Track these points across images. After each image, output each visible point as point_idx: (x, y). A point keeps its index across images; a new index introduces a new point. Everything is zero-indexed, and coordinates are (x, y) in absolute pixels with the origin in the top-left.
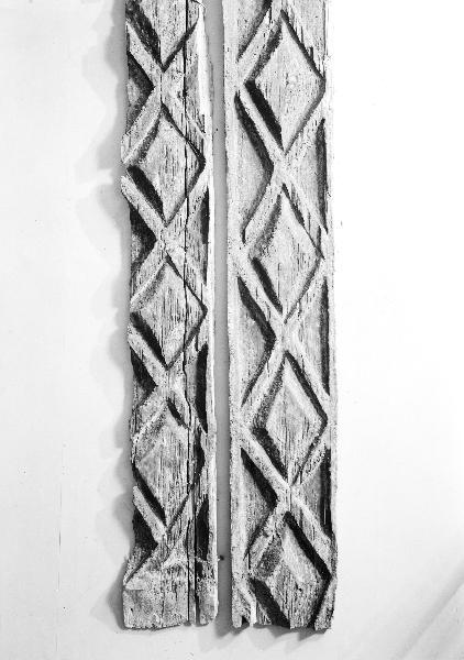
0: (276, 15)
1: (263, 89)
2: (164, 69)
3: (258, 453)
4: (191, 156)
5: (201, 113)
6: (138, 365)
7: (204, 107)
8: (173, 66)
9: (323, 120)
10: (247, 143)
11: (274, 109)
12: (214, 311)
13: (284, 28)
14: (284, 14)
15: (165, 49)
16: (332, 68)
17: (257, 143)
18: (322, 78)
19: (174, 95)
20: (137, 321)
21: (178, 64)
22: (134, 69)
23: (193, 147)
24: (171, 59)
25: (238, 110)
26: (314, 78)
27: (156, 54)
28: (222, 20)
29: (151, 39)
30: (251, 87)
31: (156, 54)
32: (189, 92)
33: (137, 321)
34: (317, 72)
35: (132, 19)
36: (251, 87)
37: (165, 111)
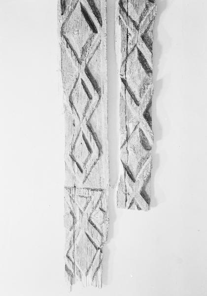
0: (83, 62)
1: (89, 28)
2: (136, 45)
3: (92, 144)
4: (125, 6)
5: (120, 26)
6: (150, 46)
7: (118, 28)
8: (132, 46)
9: (62, 14)
10: (97, 6)
11: (84, 19)
12: (115, 9)
13: (79, 56)
14: (80, 63)
15: (135, 55)
16: (58, 39)
17: (93, 6)
18: (62, 33)
19: (133, 35)
20: (148, 70)
21: (130, 47)
22: (150, 46)
23: (124, 10)
24: (133, 50)
25: (101, 18)
26: (66, 35)
27: (140, 54)
28: (107, 63)
29: (142, 60)
30: (95, 30)
31: (140, 54)
32: (126, 36)
33: (148, 70)
34: (64, 37)
35: (150, 69)
36: (95, 30)
37: (137, 27)
